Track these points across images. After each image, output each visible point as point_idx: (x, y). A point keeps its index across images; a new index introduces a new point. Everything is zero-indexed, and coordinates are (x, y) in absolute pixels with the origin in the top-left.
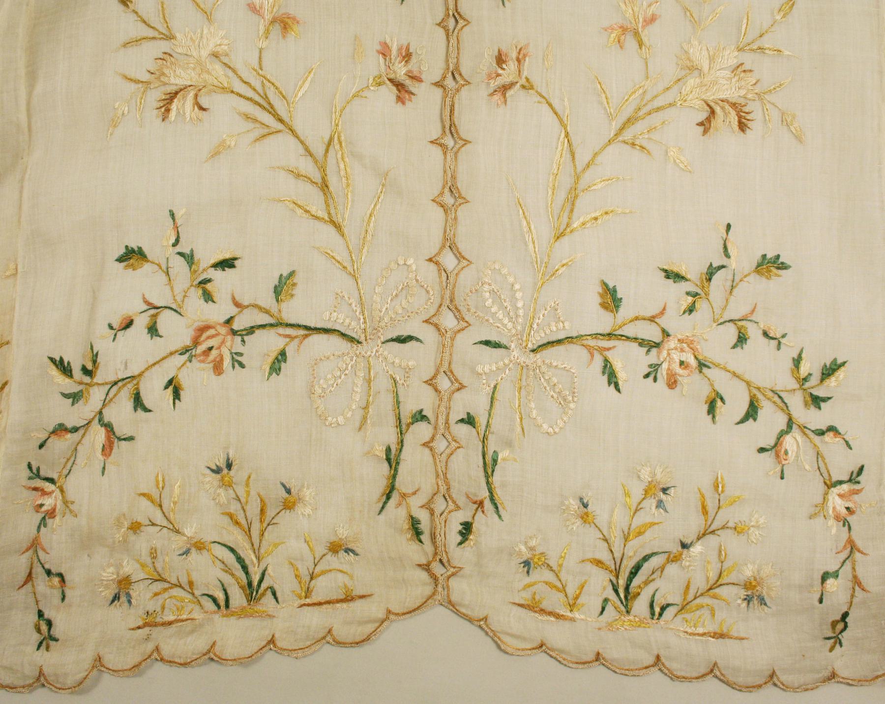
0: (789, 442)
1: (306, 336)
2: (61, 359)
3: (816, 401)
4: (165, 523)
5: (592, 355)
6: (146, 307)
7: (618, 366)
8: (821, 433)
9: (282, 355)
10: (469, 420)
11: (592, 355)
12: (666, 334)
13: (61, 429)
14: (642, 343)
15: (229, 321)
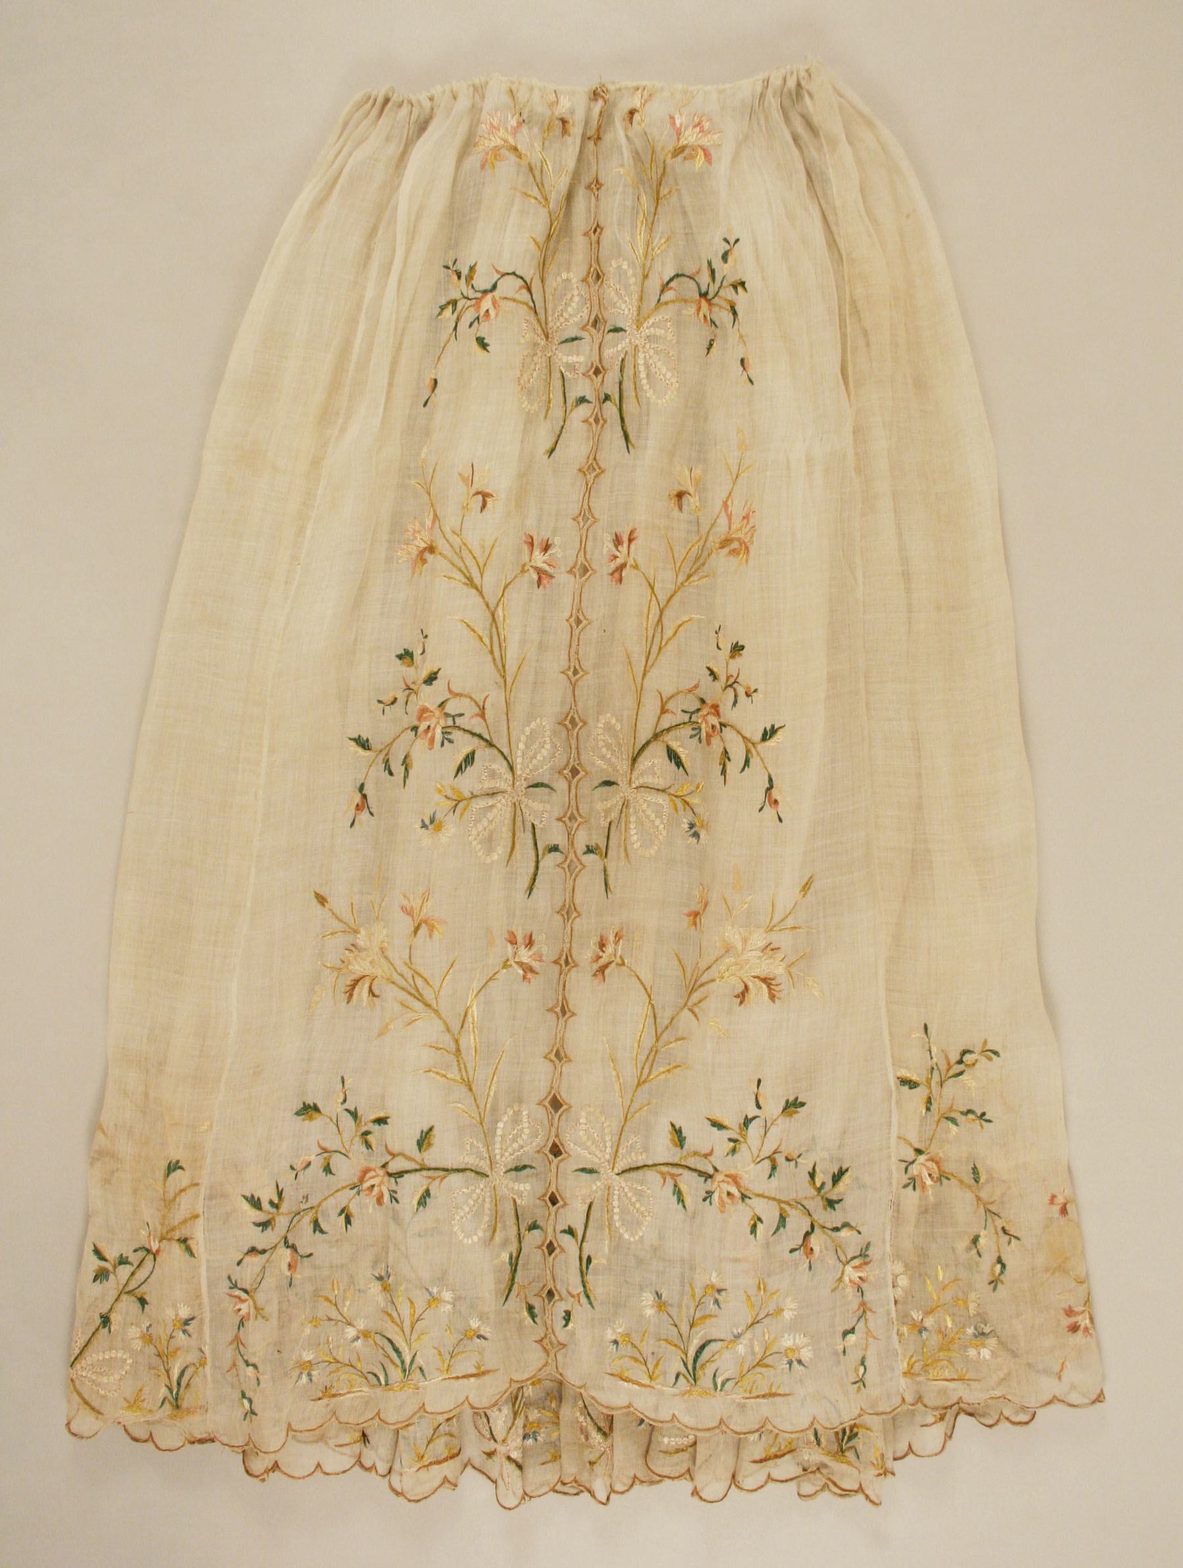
0: (815, 1241)
1: (444, 1177)
2: (253, 1196)
3: (831, 1204)
4: (340, 1317)
5: (665, 1180)
6: (320, 1151)
7: (683, 1187)
8: (837, 1229)
9: (427, 1193)
10: (570, 1231)
11: (665, 1180)
12: (716, 1170)
13: (253, 1250)
14: (701, 1173)
15: (384, 1166)
